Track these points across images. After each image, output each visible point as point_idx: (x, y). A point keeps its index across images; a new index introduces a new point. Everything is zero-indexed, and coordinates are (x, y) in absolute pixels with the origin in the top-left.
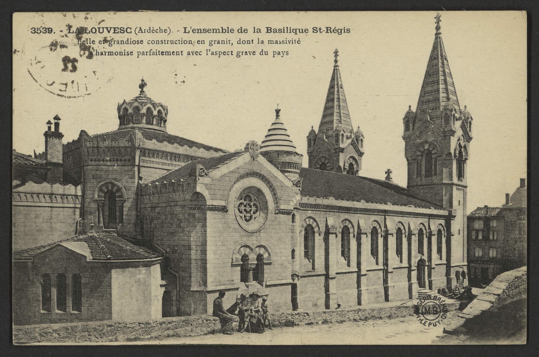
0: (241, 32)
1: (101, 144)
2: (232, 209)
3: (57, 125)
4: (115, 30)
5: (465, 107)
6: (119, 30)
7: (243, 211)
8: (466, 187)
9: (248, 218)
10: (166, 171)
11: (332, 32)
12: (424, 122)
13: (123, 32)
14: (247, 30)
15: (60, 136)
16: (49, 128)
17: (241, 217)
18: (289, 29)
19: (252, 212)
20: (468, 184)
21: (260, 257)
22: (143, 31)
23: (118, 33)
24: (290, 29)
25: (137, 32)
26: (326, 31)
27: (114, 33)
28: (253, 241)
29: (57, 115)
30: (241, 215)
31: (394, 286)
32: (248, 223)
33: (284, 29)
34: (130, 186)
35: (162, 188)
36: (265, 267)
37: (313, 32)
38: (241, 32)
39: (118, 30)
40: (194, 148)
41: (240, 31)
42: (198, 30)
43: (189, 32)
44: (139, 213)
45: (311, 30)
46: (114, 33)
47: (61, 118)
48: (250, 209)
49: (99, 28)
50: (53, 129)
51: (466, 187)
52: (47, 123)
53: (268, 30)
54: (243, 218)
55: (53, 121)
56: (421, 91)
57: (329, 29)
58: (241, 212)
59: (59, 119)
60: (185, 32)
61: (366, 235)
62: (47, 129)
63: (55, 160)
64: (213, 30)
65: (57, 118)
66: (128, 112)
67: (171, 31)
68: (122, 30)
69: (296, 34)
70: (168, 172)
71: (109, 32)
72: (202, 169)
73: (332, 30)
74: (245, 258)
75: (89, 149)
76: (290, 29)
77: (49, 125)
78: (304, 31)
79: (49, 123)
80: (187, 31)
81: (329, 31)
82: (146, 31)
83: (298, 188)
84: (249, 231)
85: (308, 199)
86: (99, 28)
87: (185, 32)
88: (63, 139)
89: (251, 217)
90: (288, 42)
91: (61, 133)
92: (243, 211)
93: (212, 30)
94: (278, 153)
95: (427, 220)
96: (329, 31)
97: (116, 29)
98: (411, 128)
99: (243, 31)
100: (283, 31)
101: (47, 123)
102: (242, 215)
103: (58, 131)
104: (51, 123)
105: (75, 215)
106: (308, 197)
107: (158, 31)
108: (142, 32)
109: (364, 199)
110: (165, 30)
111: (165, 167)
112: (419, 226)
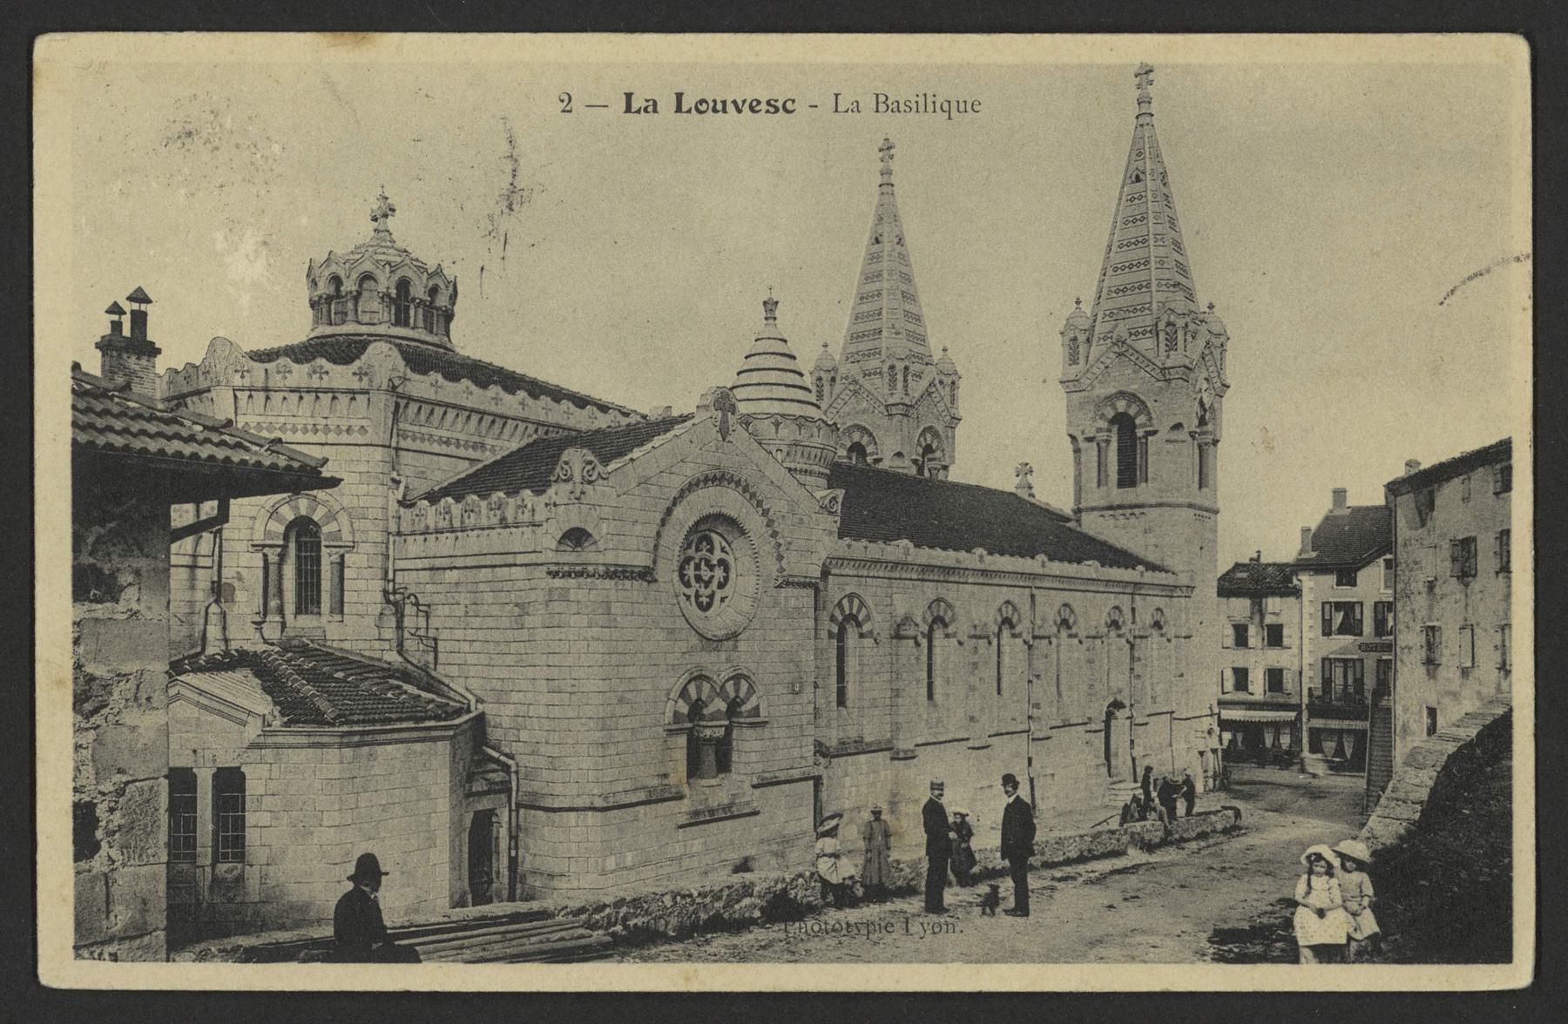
2: (667, 572)
3: (139, 319)
5: (1211, 307)
7: (693, 581)
8: (1216, 512)
9: (704, 600)
10: (466, 463)
12: (1114, 344)
15: (153, 351)
16: (116, 326)
17: (688, 597)
19: (714, 585)
20: (1220, 505)
28: (718, 665)
29: (140, 289)
30: (688, 591)
31: (1053, 775)
32: (707, 613)
34: (362, 505)
35: (466, 515)
36: (233, 646)
40: (522, 394)
44: (391, 584)
45: (667, 104)
47: (151, 297)
48: (710, 574)
50: (126, 332)
51: (1216, 512)
52: (108, 312)
54: (693, 599)
55: (128, 307)
58: (688, 585)
59: (148, 301)
61: (986, 641)
62: (107, 330)
65: (140, 297)
66: (342, 288)
70: (471, 466)
72: (590, 463)
74: (696, 708)
75: (238, 393)
77: (115, 317)
79: (115, 309)
83: (831, 518)
84: (709, 636)
85: (849, 546)
88: (159, 360)
89: (712, 596)
90: (730, 107)
91: (152, 344)
92: (693, 581)
94: (776, 421)
95: (1127, 598)
101: (108, 312)
102: (691, 592)
103: (144, 333)
104: (121, 312)
105: (193, 588)
106: (864, 542)
109: (1045, 552)
111: (462, 452)
112: (1059, 612)
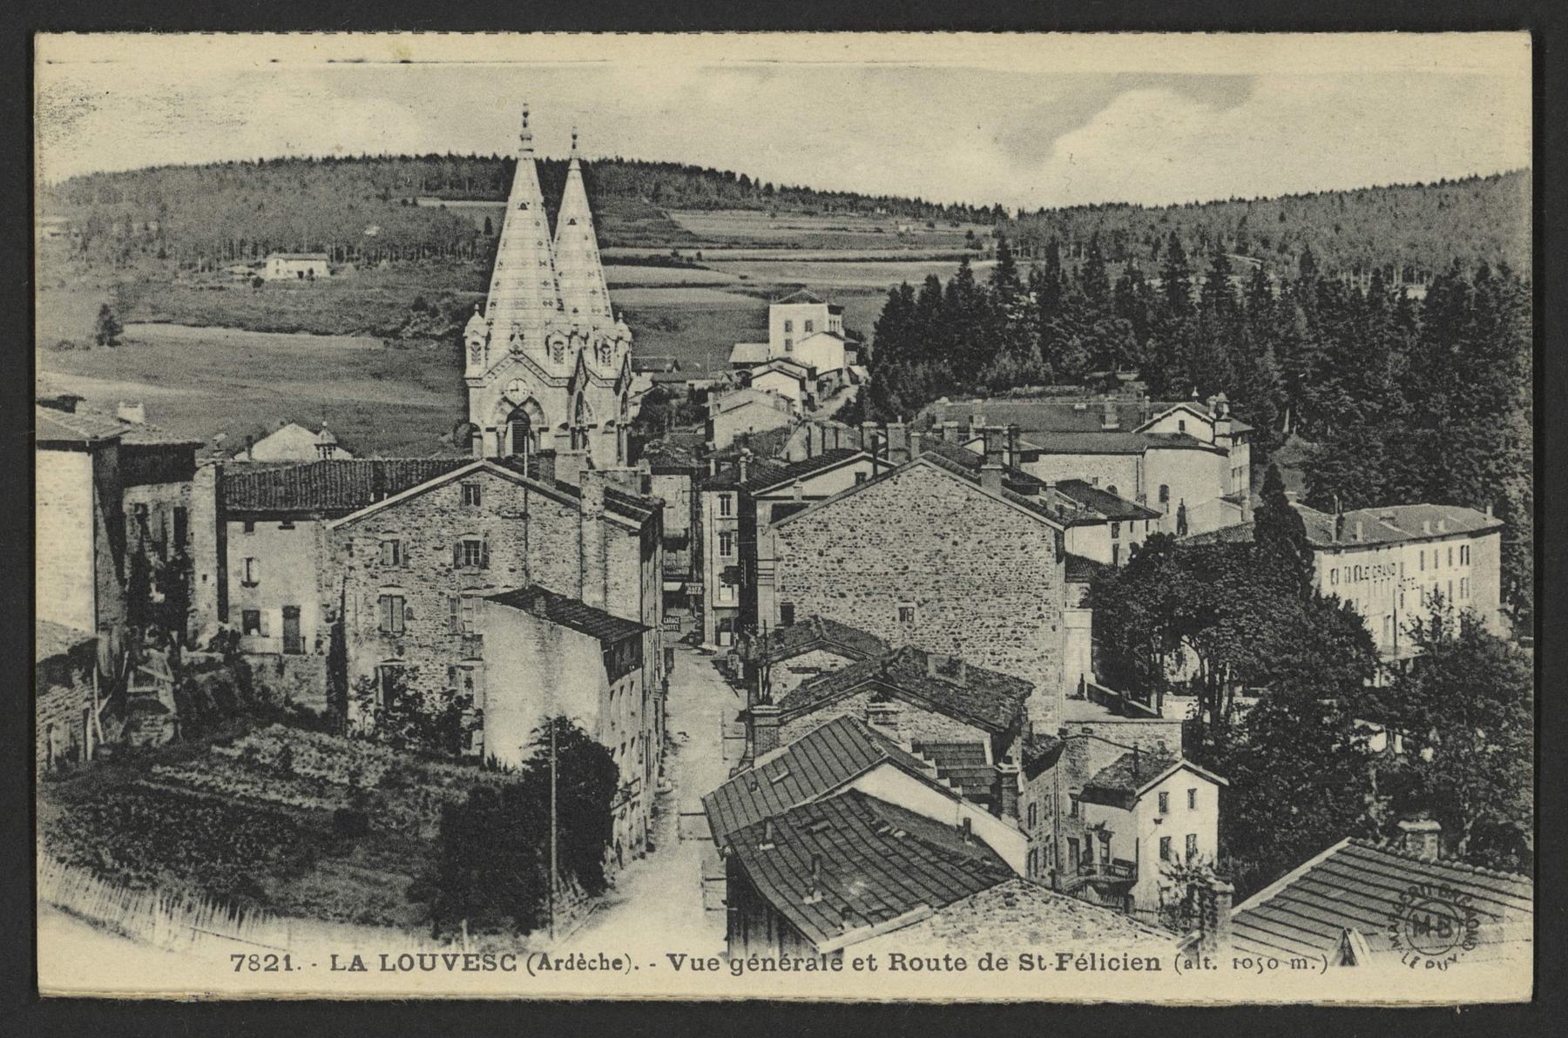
0: (990, 968)
1: (866, 467)
4: (467, 963)
6: (481, 962)
11: (908, 966)
13: (490, 966)
14: (964, 962)
18: (1098, 957)
21: (1159, 743)
22: (553, 965)
23: (477, 968)
24: (1102, 960)
25: (534, 968)
26: (1056, 964)
27: (466, 969)
37: (1021, 968)
39: (476, 963)
41: (985, 964)
42: (1149, 961)
43: (394, 969)
46: (466, 969)
49: (422, 956)
53: (894, 962)
56: (695, 171)
57: (898, 958)
60: (383, 969)
63: (715, 494)
64: (1149, 961)
67: (633, 966)
68: (1027, 962)
71: (450, 967)
73: (907, 963)
76: (1102, 960)
78: (705, 966)
80: (389, 966)
81: (898, 965)
82: (562, 965)
86: (422, 956)
87: (383, 969)
93: (1145, 963)
96: (898, 965)
97: (470, 959)
98: (171, 516)
99: (994, 965)
107: (598, 964)
108: (549, 968)
110: (618, 961)
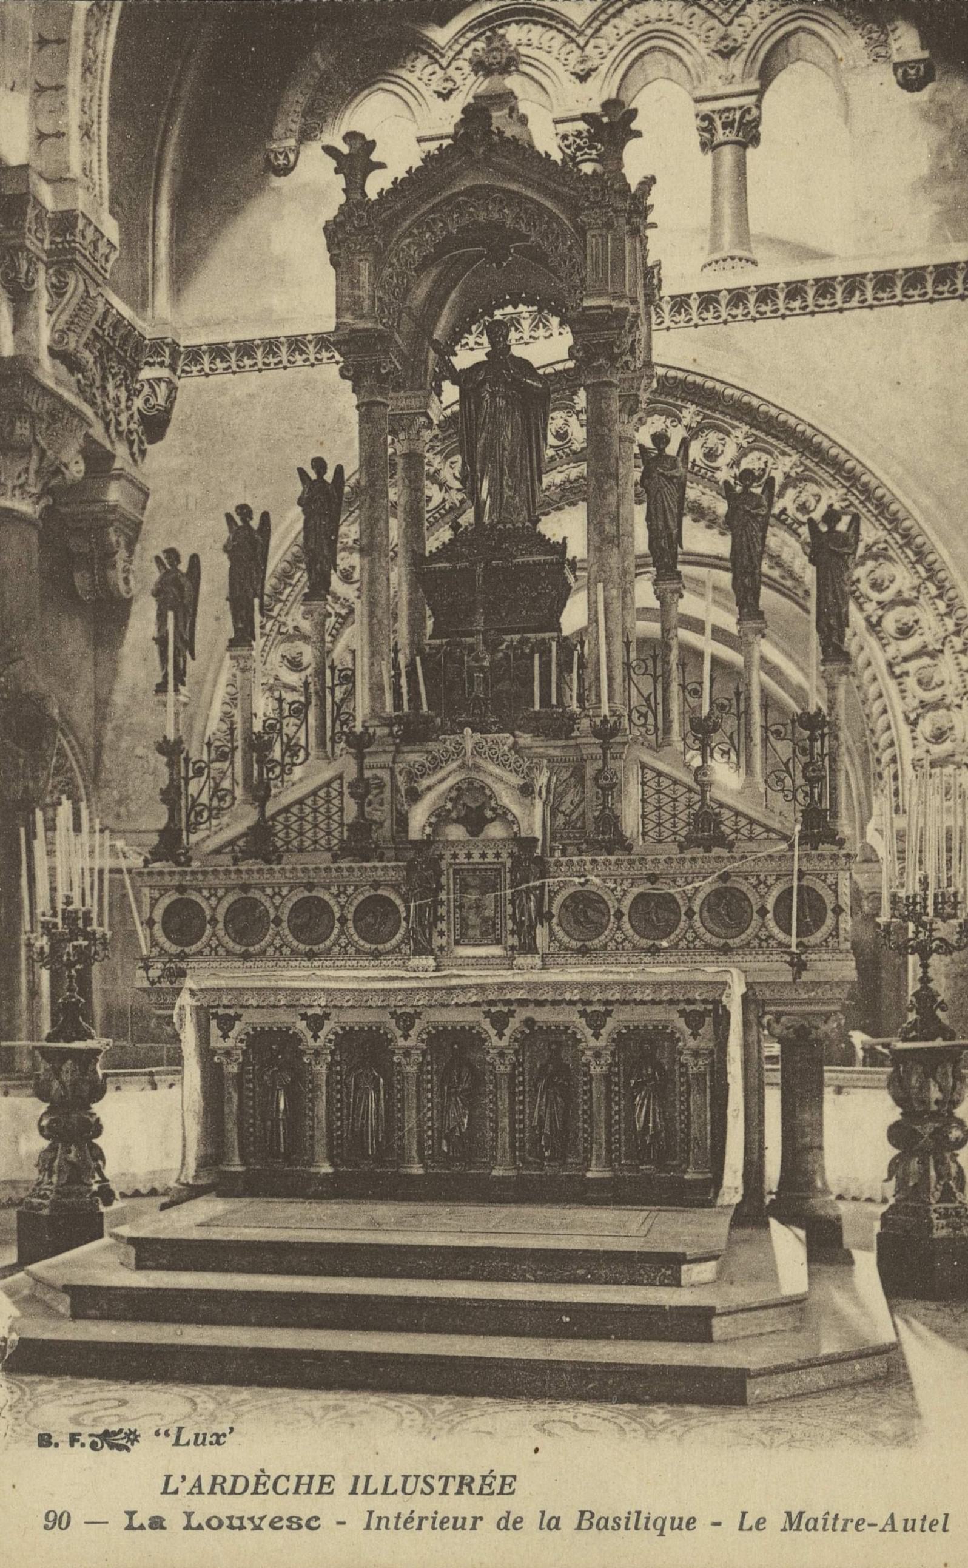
0: (506, 1528)
24: (648, 1519)
33: (826, 1520)
38: (506, 1528)
41: (503, 1522)
69: (661, 1534)
99: (510, 1526)
100: (623, 1523)
